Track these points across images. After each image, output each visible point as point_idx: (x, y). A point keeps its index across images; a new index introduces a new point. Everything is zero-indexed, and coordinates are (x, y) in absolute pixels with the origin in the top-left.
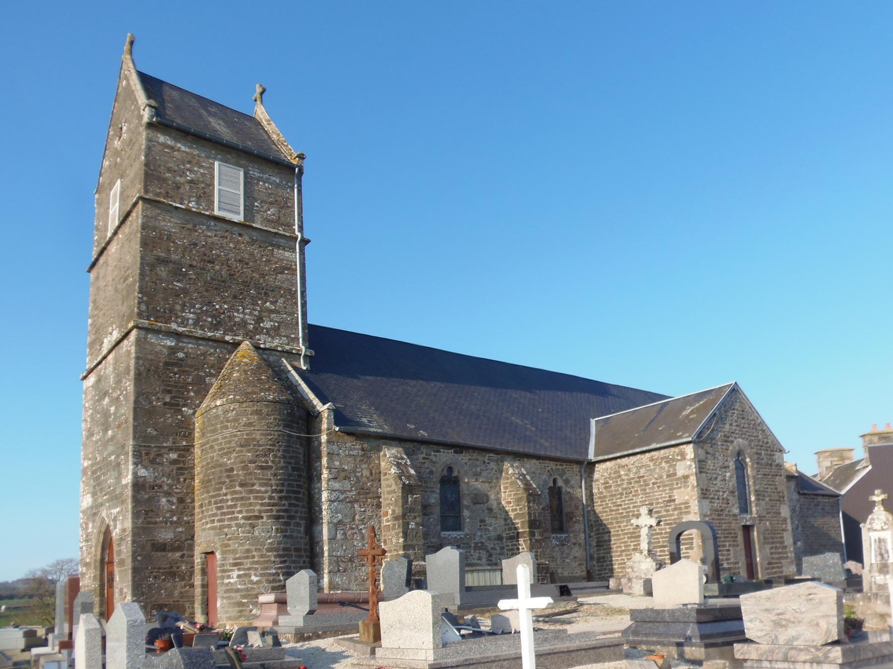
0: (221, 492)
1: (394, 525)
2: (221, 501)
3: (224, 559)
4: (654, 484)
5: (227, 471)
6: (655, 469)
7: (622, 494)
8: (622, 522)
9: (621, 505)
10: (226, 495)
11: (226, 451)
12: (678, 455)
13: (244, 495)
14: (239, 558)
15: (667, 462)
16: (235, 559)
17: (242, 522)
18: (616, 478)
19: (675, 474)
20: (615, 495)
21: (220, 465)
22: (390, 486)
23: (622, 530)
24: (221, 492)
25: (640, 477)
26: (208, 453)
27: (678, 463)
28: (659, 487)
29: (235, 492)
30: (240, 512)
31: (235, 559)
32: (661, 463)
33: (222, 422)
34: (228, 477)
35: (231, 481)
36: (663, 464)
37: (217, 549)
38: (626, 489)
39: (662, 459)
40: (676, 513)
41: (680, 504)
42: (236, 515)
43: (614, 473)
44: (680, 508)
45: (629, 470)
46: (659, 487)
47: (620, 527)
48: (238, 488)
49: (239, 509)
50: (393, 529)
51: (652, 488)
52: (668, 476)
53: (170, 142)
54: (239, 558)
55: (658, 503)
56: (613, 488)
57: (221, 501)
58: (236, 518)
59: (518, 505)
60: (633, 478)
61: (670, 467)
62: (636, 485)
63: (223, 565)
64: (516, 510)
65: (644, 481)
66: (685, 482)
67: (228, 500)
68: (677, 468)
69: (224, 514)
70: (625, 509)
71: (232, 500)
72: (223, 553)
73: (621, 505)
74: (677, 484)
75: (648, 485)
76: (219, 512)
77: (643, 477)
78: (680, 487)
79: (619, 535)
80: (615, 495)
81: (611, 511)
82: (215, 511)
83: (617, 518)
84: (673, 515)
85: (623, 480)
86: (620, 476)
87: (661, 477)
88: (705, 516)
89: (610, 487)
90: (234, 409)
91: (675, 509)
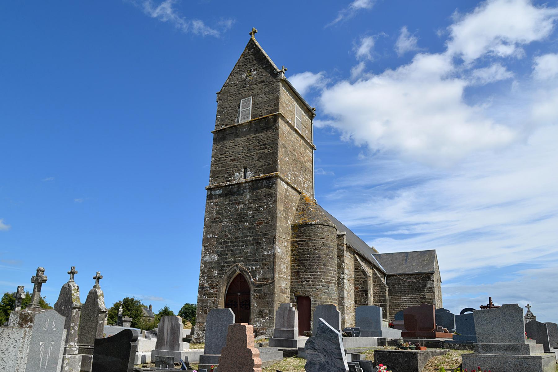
22: (360, 275)
30: (323, 279)
52: (422, 287)
72: (315, 298)
76: (312, 277)
82: (310, 276)
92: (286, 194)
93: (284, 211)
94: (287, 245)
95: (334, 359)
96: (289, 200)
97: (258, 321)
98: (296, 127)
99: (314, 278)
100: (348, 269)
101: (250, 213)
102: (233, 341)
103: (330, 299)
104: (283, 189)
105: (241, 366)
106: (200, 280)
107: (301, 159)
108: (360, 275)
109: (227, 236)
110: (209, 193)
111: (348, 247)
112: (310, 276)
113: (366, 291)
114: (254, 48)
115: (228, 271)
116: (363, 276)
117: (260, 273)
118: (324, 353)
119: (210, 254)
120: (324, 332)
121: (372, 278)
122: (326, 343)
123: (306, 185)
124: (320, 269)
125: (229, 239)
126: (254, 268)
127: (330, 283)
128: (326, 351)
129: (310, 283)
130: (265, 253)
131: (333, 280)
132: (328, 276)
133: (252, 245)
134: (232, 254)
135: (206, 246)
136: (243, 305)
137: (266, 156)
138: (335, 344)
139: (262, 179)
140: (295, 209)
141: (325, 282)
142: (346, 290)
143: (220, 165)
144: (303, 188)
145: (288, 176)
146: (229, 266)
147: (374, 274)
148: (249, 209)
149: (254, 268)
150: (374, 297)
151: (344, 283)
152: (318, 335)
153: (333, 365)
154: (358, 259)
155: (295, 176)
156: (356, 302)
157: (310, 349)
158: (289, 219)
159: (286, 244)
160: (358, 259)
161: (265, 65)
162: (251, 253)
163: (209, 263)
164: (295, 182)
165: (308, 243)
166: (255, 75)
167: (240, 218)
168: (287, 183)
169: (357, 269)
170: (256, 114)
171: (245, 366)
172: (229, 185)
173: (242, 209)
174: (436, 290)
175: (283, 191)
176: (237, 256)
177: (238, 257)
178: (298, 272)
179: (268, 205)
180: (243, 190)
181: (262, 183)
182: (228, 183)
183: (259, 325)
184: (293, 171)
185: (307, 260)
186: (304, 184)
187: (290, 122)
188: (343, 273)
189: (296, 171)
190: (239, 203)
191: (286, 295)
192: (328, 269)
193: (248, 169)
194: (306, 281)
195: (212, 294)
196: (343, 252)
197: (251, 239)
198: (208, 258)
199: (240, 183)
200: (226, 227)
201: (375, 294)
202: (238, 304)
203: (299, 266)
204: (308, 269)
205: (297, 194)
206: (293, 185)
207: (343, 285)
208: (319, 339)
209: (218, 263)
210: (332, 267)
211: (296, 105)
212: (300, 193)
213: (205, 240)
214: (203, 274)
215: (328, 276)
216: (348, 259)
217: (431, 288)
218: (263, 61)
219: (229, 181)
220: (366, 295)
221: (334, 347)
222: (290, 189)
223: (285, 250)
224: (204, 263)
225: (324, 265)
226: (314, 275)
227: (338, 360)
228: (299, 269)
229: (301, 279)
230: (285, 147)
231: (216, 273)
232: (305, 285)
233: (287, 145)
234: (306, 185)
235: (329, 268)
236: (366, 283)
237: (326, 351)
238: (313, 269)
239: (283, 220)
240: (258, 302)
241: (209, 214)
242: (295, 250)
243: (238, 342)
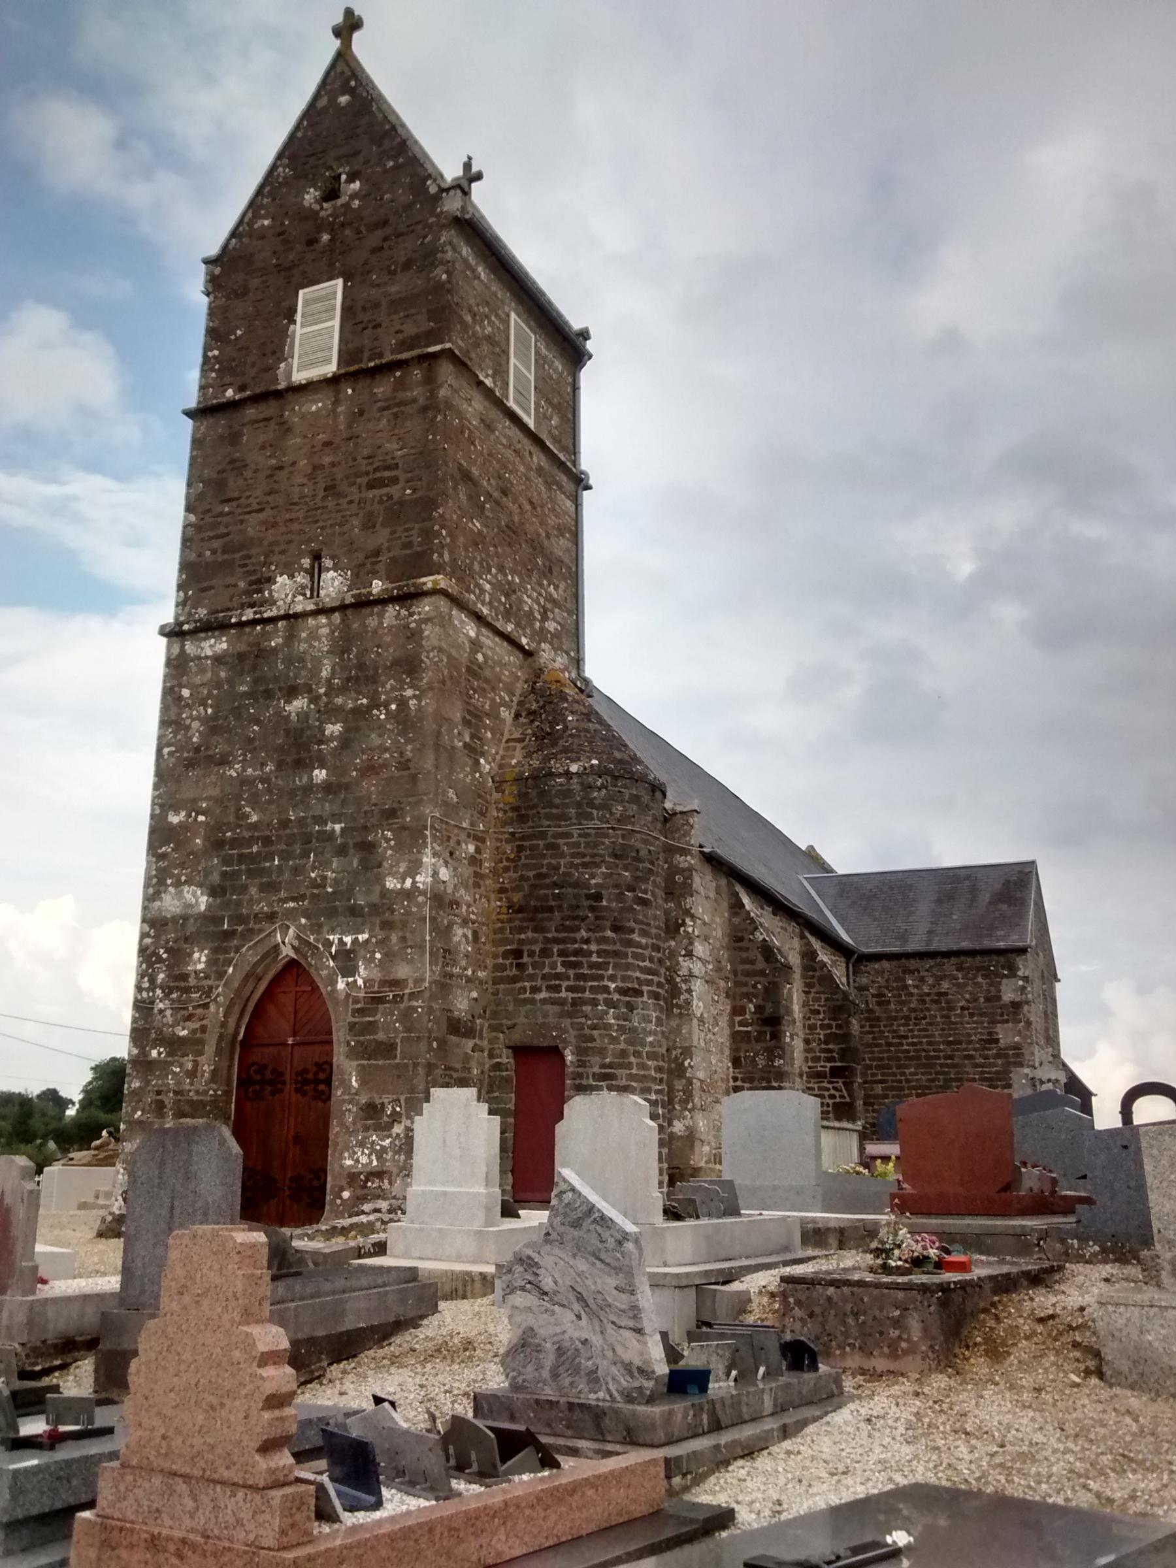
0: (578, 936)
1: (760, 1033)
2: (577, 953)
3: (582, 1064)
4: (962, 1008)
5: (588, 897)
6: (966, 985)
7: (907, 1018)
8: (908, 1067)
9: (906, 1037)
10: (587, 941)
11: (587, 859)
12: (1003, 968)
13: (618, 947)
14: (610, 1066)
15: (985, 976)
16: (603, 1066)
17: (616, 997)
18: (898, 989)
19: (999, 998)
20: (895, 1018)
21: (576, 885)
22: (753, 962)
23: (908, 1081)
24: (578, 936)
25: (940, 994)
26: (543, 856)
27: (1005, 981)
28: (971, 1015)
29: (605, 940)
30: (612, 978)
31: (603, 1066)
32: (975, 977)
33: (579, 805)
34: (592, 909)
35: (597, 918)
36: (980, 979)
37: (566, 1043)
38: (915, 1010)
39: (978, 969)
40: (1000, 1061)
41: (1006, 1049)
42: (606, 983)
43: (895, 981)
44: (1007, 1056)
45: (922, 979)
46: (971, 1015)
47: (903, 1074)
48: (609, 933)
49: (610, 972)
50: (758, 1040)
51: (961, 1016)
52: (987, 1000)
53: (472, 260)
54: (610, 1066)
55: (970, 1042)
56: (893, 1006)
57: (577, 953)
58: (606, 989)
59: (834, 1019)
60: (928, 994)
61: (991, 984)
62: (934, 1006)
63: (580, 1076)
64: (829, 1027)
65: (947, 1002)
66: (1015, 1013)
67: (590, 953)
68: (1003, 988)
69: (579, 977)
70: (913, 1044)
71: (600, 953)
72: (580, 1051)
73: (906, 1037)
74: (1002, 1015)
75: (954, 1009)
76: (571, 972)
77: (946, 994)
78: (1007, 1021)
79: (902, 1089)
80: (895, 1018)
81: (889, 1044)
82: (560, 969)
83: (898, 1059)
84: (994, 1065)
85: (911, 995)
86: (905, 987)
87: (976, 1000)
88: (817, 1059)
89: (889, 1003)
90: (603, 786)
91: (997, 1056)
92: (473, 661)
93: (466, 723)
94: (478, 850)
95: (610, 1329)
96: (487, 681)
97: (362, 1144)
98: (511, 404)
99: (579, 977)
100: (706, 939)
101: (333, 729)
102: (187, 1299)
103: (637, 1054)
104: (462, 639)
105: (215, 1401)
106: (139, 988)
107: (533, 526)
108: (753, 962)
109: (247, 817)
110: (176, 650)
111: (713, 861)
112: (560, 969)
113: (773, 1020)
114: (352, 92)
115: (249, 954)
116: (761, 964)
117: (373, 958)
118: (577, 1307)
119: (178, 884)
120: (576, 1224)
121: (797, 975)
122: (582, 1265)
123: (551, 626)
124: (600, 941)
125: (254, 826)
126: (348, 940)
127: (638, 993)
128: (581, 1298)
129: (563, 994)
130: (391, 883)
131: (649, 983)
132: (628, 967)
133: (342, 851)
134: (263, 888)
135: (163, 856)
136: (306, 1082)
137: (396, 512)
138: (617, 1270)
139: (383, 601)
140: (506, 714)
141: (618, 990)
142: (701, 1020)
143: (217, 544)
144: (541, 635)
145: (482, 591)
146: (251, 931)
147: (809, 955)
148: (331, 713)
149: (348, 940)
150: (807, 1041)
151: (689, 991)
152: (554, 1236)
153: (610, 1354)
154: (746, 900)
155: (510, 591)
156: (736, 1062)
157: (523, 1289)
158: (483, 754)
159: (471, 848)
160: (746, 900)
161: (395, 158)
162: (336, 882)
163: (174, 919)
164: (508, 615)
165: (551, 847)
166: (353, 196)
167: (299, 748)
168: (479, 618)
169: (740, 936)
170: (360, 351)
171: (228, 1402)
172: (253, 623)
173: (303, 716)
174: (1034, 1012)
175: (459, 647)
176: (283, 894)
177: (286, 900)
178: (518, 954)
179: (403, 703)
180: (307, 640)
181: (381, 616)
182: (248, 615)
183: (364, 1160)
184: (501, 569)
185: (550, 909)
186: (545, 618)
187: (488, 382)
188: (690, 954)
189: (513, 572)
190: (292, 692)
191: (470, 1043)
192: (630, 943)
193: (327, 562)
194: (549, 988)
195: (183, 1041)
196: (690, 877)
197: (338, 827)
198: (170, 904)
199: (296, 616)
200: (243, 781)
201: (812, 1028)
202: (287, 1077)
203: (522, 930)
204: (556, 941)
205: (513, 658)
206: (499, 625)
207: (688, 1003)
208: (557, 1251)
209: (211, 918)
210: (644, 933)
211: (513, 316)
212: (528, 654)
213: (160, 834)
214: (150, 965)
215: (628, 967)
216: (706, 908)
217: (1016, 1006)
218: (387, 144)
219: (252, 606)
220: (776, 1036)
221: (612, 1282)
222: (489, 640)
223: (467, 871)
224: (154, 924)
225: (616, 929)
226: (577, 965)
227: (628, 1334)
228: (521, 941)
229: (532, 977)
230: (467, 477)
231: (200, 960)
232: (544, 1001)
233: (475, 472)
234: (551, 626)
235: (636, 937)
236: (772, 992)
237: (581, 1298)
238: (574, 941)
239: (464, 758)
240: (362, 1072)
241: (175, 733)
242: (506, 869)
243: (205, 1303)
